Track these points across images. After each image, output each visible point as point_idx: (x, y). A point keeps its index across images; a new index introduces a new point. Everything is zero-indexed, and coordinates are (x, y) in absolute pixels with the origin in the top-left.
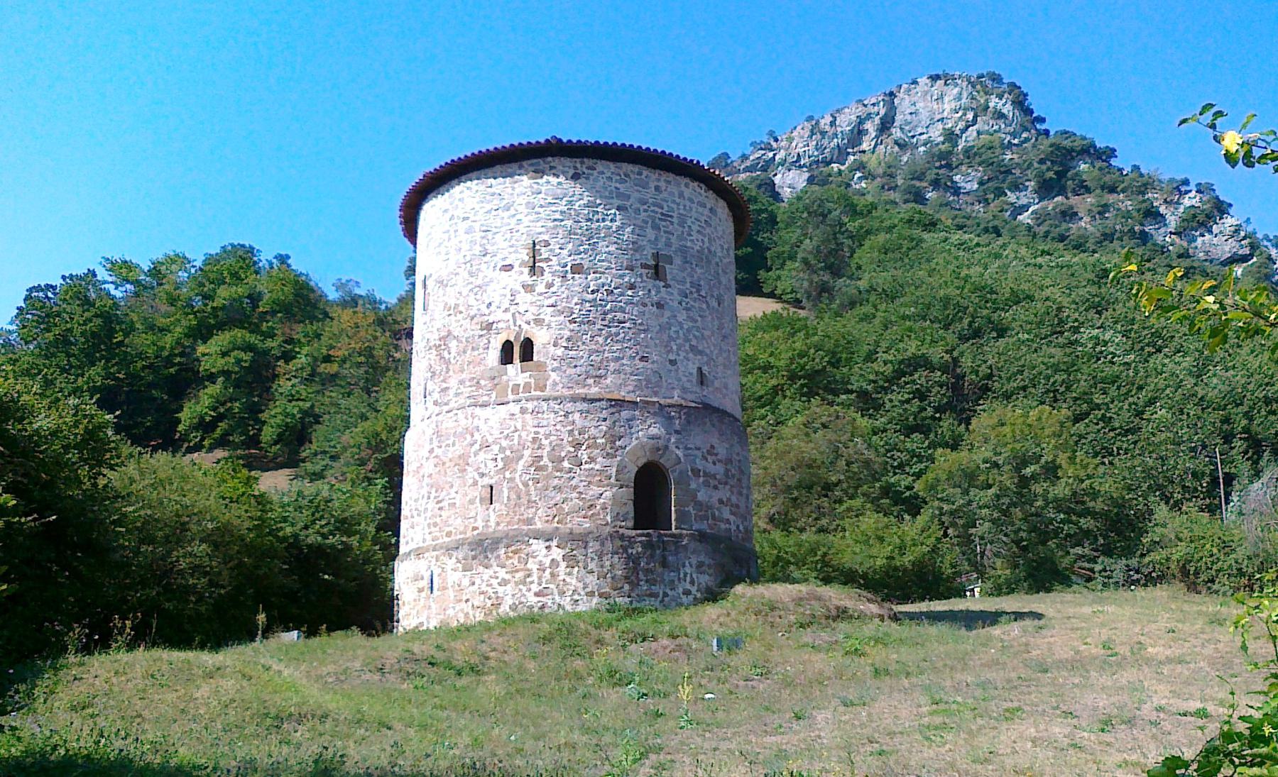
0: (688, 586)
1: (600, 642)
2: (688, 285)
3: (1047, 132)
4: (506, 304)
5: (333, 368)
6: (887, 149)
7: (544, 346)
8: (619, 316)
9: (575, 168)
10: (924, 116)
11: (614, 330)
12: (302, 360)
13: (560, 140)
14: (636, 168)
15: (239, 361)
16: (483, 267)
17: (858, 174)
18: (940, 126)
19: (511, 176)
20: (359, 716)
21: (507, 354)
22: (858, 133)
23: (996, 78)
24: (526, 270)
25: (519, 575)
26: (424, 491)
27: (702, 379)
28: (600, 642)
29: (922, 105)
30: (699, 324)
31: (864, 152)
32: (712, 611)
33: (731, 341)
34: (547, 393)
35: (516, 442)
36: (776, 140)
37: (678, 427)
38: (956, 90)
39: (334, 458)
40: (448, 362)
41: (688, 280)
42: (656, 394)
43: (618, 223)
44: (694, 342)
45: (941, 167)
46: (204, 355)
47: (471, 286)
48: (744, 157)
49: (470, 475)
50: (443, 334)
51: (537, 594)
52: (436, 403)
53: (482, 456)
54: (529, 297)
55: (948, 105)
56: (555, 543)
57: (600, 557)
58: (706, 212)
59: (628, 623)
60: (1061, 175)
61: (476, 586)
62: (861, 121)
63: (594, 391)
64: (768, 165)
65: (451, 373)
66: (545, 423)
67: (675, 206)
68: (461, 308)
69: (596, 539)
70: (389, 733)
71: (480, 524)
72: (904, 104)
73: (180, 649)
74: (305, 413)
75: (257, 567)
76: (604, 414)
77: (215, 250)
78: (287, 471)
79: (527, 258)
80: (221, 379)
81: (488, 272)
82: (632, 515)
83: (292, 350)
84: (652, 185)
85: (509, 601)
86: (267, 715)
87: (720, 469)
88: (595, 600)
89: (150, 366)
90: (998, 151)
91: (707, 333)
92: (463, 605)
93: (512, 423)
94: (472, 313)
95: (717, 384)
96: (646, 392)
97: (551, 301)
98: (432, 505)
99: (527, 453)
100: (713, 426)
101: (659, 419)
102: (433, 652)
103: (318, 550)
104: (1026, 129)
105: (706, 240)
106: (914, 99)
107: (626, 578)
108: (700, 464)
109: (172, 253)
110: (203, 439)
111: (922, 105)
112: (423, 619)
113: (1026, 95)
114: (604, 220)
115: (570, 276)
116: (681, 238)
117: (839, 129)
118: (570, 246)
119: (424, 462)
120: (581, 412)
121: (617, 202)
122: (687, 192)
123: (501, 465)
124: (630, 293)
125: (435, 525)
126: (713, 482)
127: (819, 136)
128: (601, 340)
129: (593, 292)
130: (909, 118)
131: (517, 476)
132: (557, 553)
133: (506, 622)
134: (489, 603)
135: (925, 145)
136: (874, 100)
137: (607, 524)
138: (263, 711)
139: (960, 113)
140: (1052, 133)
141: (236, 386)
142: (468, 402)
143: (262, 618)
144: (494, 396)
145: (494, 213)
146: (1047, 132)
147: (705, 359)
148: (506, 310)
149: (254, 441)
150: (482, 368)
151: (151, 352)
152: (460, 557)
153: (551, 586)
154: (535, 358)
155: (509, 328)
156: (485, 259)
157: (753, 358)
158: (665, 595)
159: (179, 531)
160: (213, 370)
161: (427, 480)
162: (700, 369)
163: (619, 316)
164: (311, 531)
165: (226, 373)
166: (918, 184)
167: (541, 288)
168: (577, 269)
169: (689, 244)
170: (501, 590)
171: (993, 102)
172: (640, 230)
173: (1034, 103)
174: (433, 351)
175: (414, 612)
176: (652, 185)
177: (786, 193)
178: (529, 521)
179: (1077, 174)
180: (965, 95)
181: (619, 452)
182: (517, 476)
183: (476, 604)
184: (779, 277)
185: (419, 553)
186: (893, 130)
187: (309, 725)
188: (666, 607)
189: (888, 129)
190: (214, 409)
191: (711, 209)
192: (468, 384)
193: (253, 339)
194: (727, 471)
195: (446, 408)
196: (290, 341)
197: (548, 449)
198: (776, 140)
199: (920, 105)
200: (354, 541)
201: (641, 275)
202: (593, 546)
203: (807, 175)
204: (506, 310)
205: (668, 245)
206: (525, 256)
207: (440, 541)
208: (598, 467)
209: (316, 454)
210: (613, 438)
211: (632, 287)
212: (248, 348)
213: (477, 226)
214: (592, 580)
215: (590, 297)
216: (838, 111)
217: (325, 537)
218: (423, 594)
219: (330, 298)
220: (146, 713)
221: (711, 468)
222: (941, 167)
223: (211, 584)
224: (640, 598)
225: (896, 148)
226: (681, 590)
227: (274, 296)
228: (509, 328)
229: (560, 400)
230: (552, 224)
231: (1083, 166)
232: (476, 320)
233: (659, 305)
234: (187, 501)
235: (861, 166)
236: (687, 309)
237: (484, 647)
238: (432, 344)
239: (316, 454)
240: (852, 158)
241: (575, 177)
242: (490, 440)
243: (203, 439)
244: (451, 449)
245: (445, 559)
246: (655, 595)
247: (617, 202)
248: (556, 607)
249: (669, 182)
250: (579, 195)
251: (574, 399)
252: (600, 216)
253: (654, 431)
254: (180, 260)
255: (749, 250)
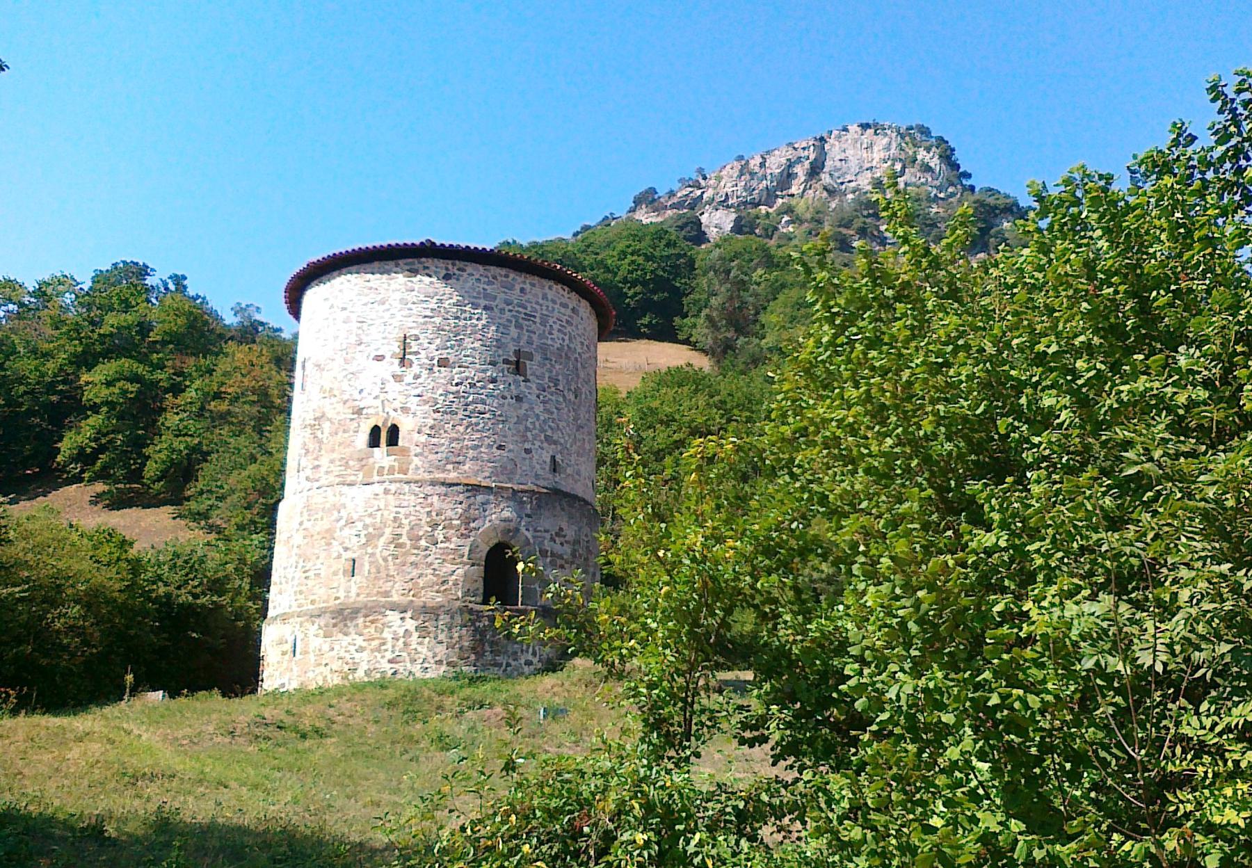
0: (530, 658)
1: (440, 708)
2: (547, 380)
3: (972, 188)
4: (376, 392)
5: (224, 407)
6: (815, 194)
7: (410, 432)
8: (480, 407)
9: (447, 269)
10: (853, 165)
11: (474, 420)
12: (191, 394)
13: (434, 244)
14: (503, 271)
15: (124, 392)
16: (358, 355)
17: (786, 218)
18: (869, 174)
19: (388, 272)
20: (201, 776)
21: (374, 441)
22: (787, 177)
23: (925, 131)
24: (397, 361)
25: (376, 643)
26: (295, 558)
27: (555, 467)
28: (440, 708)
29: (852, 152)
30: (555, 416)
31: (793, 195)
32: (549, 680)
33: (586, 429)
34: (410, 476)
35: (378, 520)
36: (705, 178)
37: (529, 512)
38: (886, 140)
39: (221, 498)
40: (320, 442)
41: (547, 375)
42: (510, 480)
43: (484, 322)
44: (549, 433)
45: (869, 216)
46: (88, 383)
47: (345, 373)
48: (672, 194)
49: (335, 549)
50: (318, 415)
51: (390, 661)
52: (307, 479)
53: (347, 531)
54: (398, 387)
55: (878, 154)
56: (409, 614)
57: (450, 629)
58: (569, 312)
59: (468, 691)
60: (984, 232)
61: (335, 652)
62: (791, 164)
63: (452, 476)
64: (696, 203)
65: (323, 452)
66: (405, 504)
67: (538, 307)
68: (336, 392)
69: (447, 612)
70: (225, 791)
71: (342, 594)
72: (834, 150)
73: (56, 715)
74: (194, 449)
75: (128, 627)
76: (461, 498)
77: (106, 266)
78: (170, 509)
79: (398, 350)
80: (105, 409)
81: (362, 360)
82: (481, 591)
83: (180, 383)
84: (518, 287)
85: (364, 667)
86: (124, 774)
87: (567, 549)
88: (444, 668)
89: (32, 392)
90: (924, 204)
91: (561, 424)
92: (322, 668)
93: (376, 503)
94: (345, 397)
95: (569, 471)
96: (502, 478)
97: (418, 392)
98: (299, 574)
99: (388, 531)
100: (563, 509)
101: (512, 503)
102: (283, 716)
103: (188, 609)
104: (952, 185)
105: (567, 338)
106: (845, 146)
107: (473, 649)
108: (547, 545)
109: (59, 274)
110: (83, 471)
111: (852, 152)
112: (285, 680)
113: (953, 150)
114: (471, 319)
115: (436, 369)
116: (541, 336)
117: (769, 171)
118: (438, 341)
119: (294, 533)
120: (439, 495)
121: (483, 302)
122: (550, 295)
123: (363, 540)
124: (491, 386)
125: (301, 592)
126: (559, 562)
127: (748, 177)
128: (461, 429)
129: (457, 385)
130: (838, 164)
131: (378, 551)
132: (411, 624)
133: (360, 688)
134: (346, 668)
135: (854, 192)
136: (804, 145)
137: (458, 599)
138: (122, 771)
139: (889, 163)
140: (977, 190)
141: (120, 417)
142: (338, 480)
143: (129, 678)
144: (361, 475)
145: (370, 306)
146: (972, 188)
147: (559, 448)
148: (376, 397)
149: (136, 475)
150: (352, 449)
151: (33, 378)
152: (322, 624)
153: (404, 654)
154: (400, 443)
155: (377, 414)
156: (359, 348)
157: (653, 411)
158: (508, 665)
159: (51, 593)
160: (98, 401)
161: (296, 550)
162: (553, 458)
163: (480, 407)
164: (183, 591)
165: (111, 405)
166: (844, 231)
167: (409, 378)
168: (443, 363)
169: (549, 342)
170: (357, 656)
171: (922, 154)
172: (503, 328)
173: (959, 156)
174: (308, 430)
175: (277, 673)
176: (518, 287)
177: (712, 233)
178: (387, 594)
179: (999, 232)
180: (894, 145)
181: (473, 533)
182: (378, 551)
183: (335, 668)
184: (694, 326)
185: (284, 618)
186: (823, 176)
187: (159, 782)
188: (509, 676)
189: (818, 174)
190: (96, 440)
191: (573, 310)
192: (338, 463)
193: (141, 369)
194: (574, 551)
195: (316, 484)
196: (180, 373)
197: (407, 528)
198: (705, 178)
199: (850, 152)
200: (225, 600)
201: (503, 371)
202: (444, 619)
203: (734, 216)
204: (376, 397)
205: (530, 343)
206: (396, 348)
207: (305, 608)
208: (452, 546)
209: (201, 493)
210: (467, 520)
211: (493, 381)
212: (135, 378)
213: (354, 317)
214: (441, 650)
215: (455, 389)
216: (768, 153)
217: (196, 596)
218: (287, 657)
219: (227, 322)
220: (26, 771)
221: (558, 548)
222: (869, 216)
223: (86, 643)
224: (485, 667)
225: (825, 194)
226: (523, 661)
227: (167, 326)
228: (377, 414)
229: (420, 483)
230: (422, 320)
231: (1005, 224)
232: (348, 404)
233: (519, 399)
234: (60, 565)
235: (789, 210)
236: (544, 402)
237: (331, 712)
238: (307, 422)
239: (201, 493)
240: (780, 201)
241: (447, 277)
242: (355, 517)
243: (83, 471)
244: (319, 523)
245: (308, 625)
246: (500, 665)
247: (483, 302)
248: (407, 674)
249: (533, 285)
250: (449, 295)
251: (433, 483)
252: (468, 315)
253: (507, 514)
254: (63, 281)
255: (666, 294)
